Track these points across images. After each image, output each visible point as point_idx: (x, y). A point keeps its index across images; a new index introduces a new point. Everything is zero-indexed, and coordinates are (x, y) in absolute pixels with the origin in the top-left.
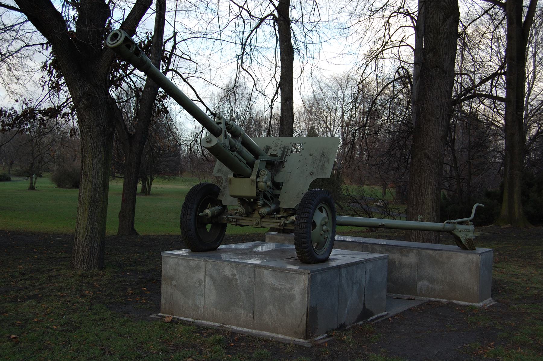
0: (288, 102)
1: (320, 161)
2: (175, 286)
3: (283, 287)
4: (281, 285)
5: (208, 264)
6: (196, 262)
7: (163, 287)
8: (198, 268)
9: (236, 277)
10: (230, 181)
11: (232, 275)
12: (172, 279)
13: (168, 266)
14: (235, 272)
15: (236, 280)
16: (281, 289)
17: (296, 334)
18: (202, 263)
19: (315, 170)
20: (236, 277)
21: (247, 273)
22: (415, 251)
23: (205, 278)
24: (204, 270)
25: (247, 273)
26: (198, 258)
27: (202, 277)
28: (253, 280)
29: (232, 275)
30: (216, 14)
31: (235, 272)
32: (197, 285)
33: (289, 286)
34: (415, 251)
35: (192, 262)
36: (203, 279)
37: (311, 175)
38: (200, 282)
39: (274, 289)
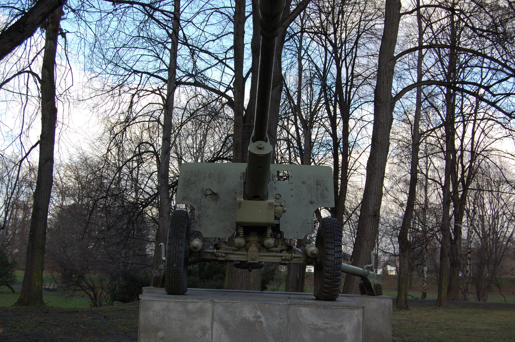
0: (49, 163)
1: (317, 190)
3: (328, 326)
4: (326, 323)
6: (198, 305)
8: (201, 312)
9: (261, 319)
10: (240, 204)
11: (254, 317)
12: (158, 330)
13: (151, 313)
14: (259, 313)
16: (327, 328)
18: (208, 306)
19: (314, 199)
20: (261, 319)
21: (277, 313)
23: (212, 324)
24: (211, 313)
25: (277, 313)
27: (207, 323)
28: (286, 321)
29: (254, 317)
31: (259, 313)
32: (199, 334)
33: (337, 324)
37: (312, 203)
39: (317, 329)
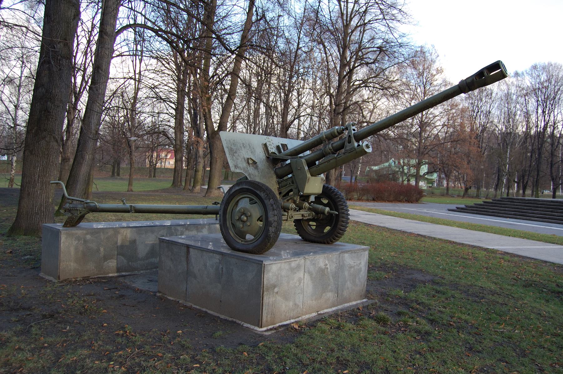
2: (277, 293)
5: (307, 260)
6: (297, 262)
7: (265, 298)
8: (298, 267)
12: (275, 286)
13: (270, 274)
15: (327, 268)
17: (361, 297)
22: (207, 227)
26: (299, 258)
30: (306, 11)
31: (327, 262)
34: (207, 227)
35: (293, 262)
36: (302, 277)
38: (300, 280)
